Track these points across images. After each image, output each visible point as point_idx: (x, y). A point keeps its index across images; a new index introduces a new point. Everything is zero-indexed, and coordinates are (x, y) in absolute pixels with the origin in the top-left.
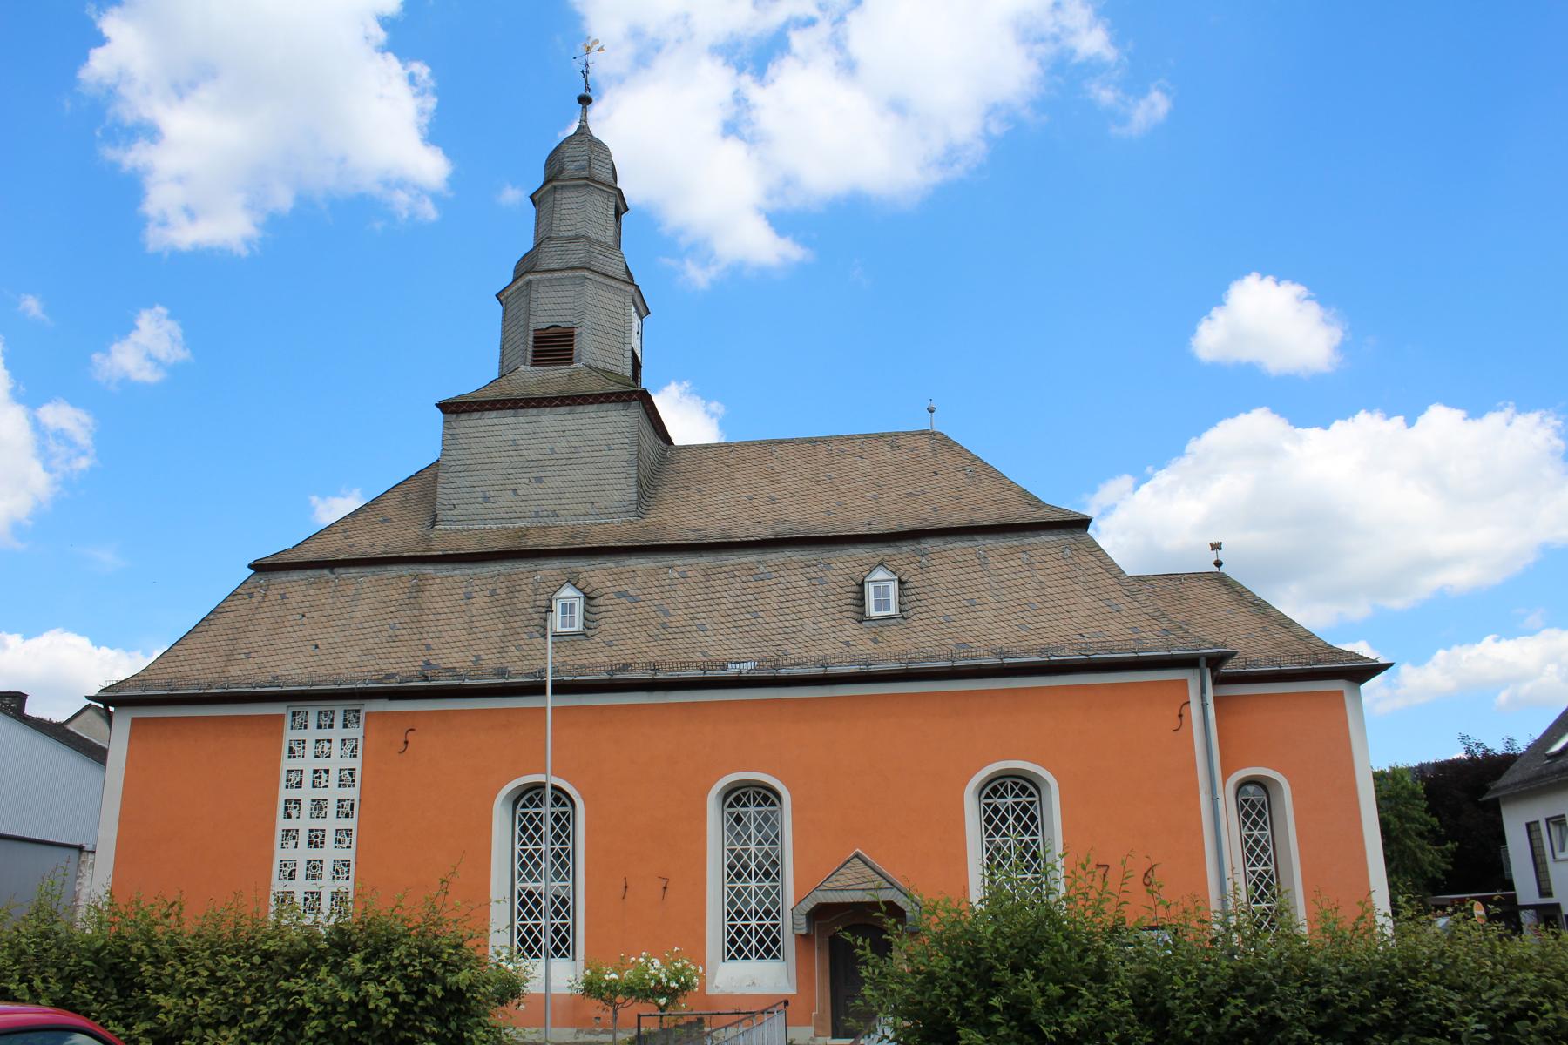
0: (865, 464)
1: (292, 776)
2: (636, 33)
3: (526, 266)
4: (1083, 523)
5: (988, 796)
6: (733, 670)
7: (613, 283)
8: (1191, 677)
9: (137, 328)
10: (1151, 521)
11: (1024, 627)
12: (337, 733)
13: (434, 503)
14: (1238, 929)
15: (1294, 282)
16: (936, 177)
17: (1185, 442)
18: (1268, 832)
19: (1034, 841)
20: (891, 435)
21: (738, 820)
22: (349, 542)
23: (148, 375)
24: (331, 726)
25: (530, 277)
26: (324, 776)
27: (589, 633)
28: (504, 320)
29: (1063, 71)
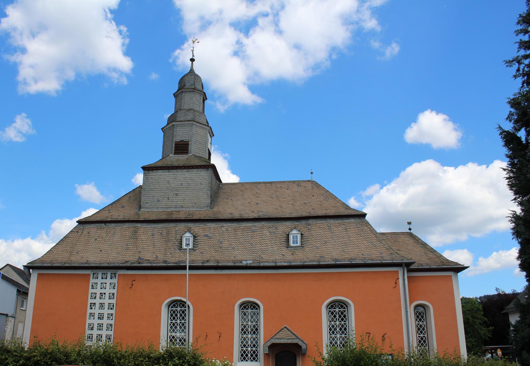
0: (289, 191)
1: (93, 295)
2: (202, 18)
3: (172, 119)
4: (364, 215)
5: (330, 308)
6: (244, 263)
7: (202, 126)
8: (400, 270)
9: (15, 122)
10: (386, 203)
11: (343, 251)
12: (108, 281)
13: (140, 201)
14: (413, 357)
15: (444, 114)
16: (310, 74)
17: (400, 173)
18: (425, 323)
19: (345, 324)
20: (298, 181)
21: (245, 314)
22: (111, 214)
23: (18, 139)
24: (106, 278)
25: (174, 123)
26: (104, 295)
27: (195, 249)
28: (164, 137)
29: (359, 35)
